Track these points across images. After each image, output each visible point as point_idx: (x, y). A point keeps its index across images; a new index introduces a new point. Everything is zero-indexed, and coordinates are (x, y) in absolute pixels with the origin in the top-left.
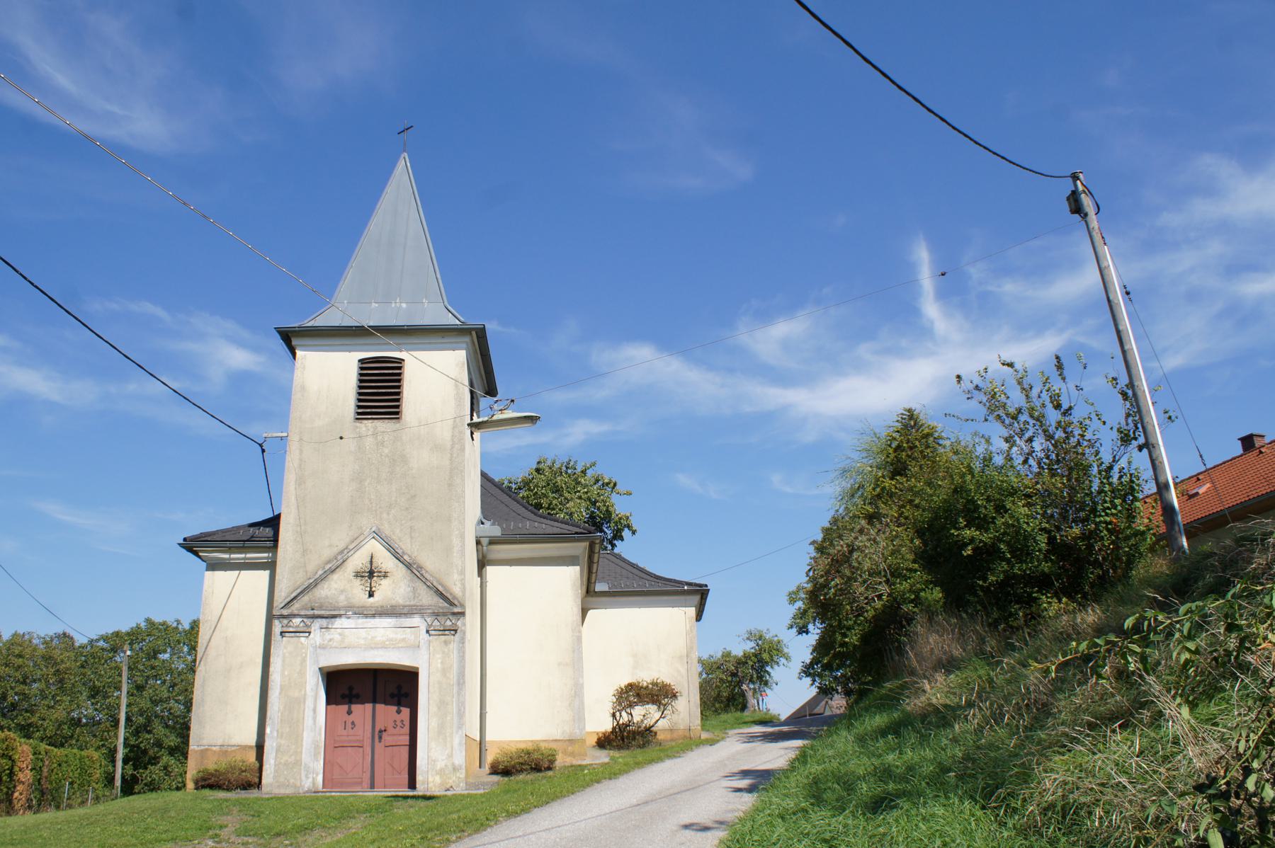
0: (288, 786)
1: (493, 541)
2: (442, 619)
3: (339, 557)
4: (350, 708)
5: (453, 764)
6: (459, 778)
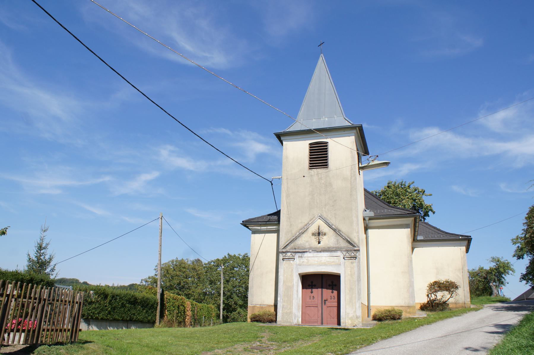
0: (287, 322)
1: (371, 218)
2: (350, 253)
3: (305, 227)
4: (312, 290)
5: (356, 315)
6: (359, 321)
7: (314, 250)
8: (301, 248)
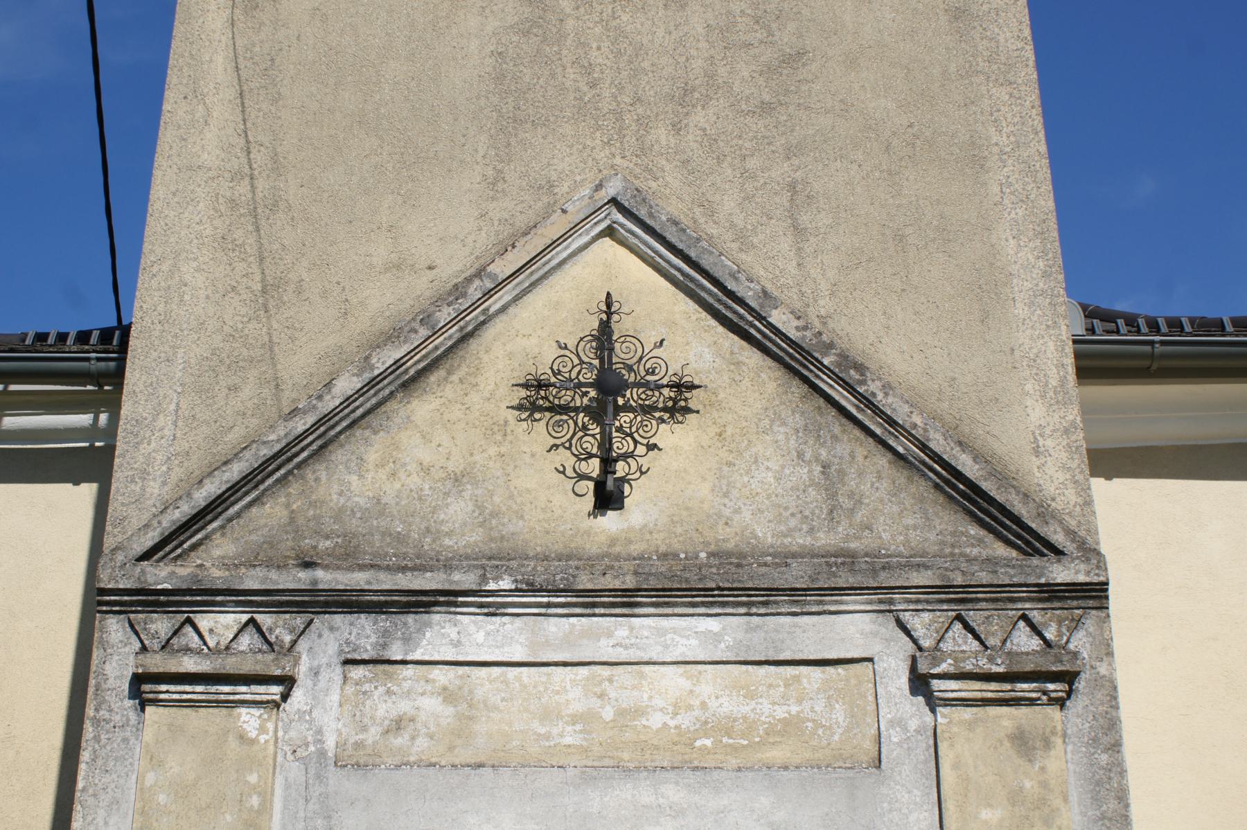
7: (539, 580)
8: (375, 555)
